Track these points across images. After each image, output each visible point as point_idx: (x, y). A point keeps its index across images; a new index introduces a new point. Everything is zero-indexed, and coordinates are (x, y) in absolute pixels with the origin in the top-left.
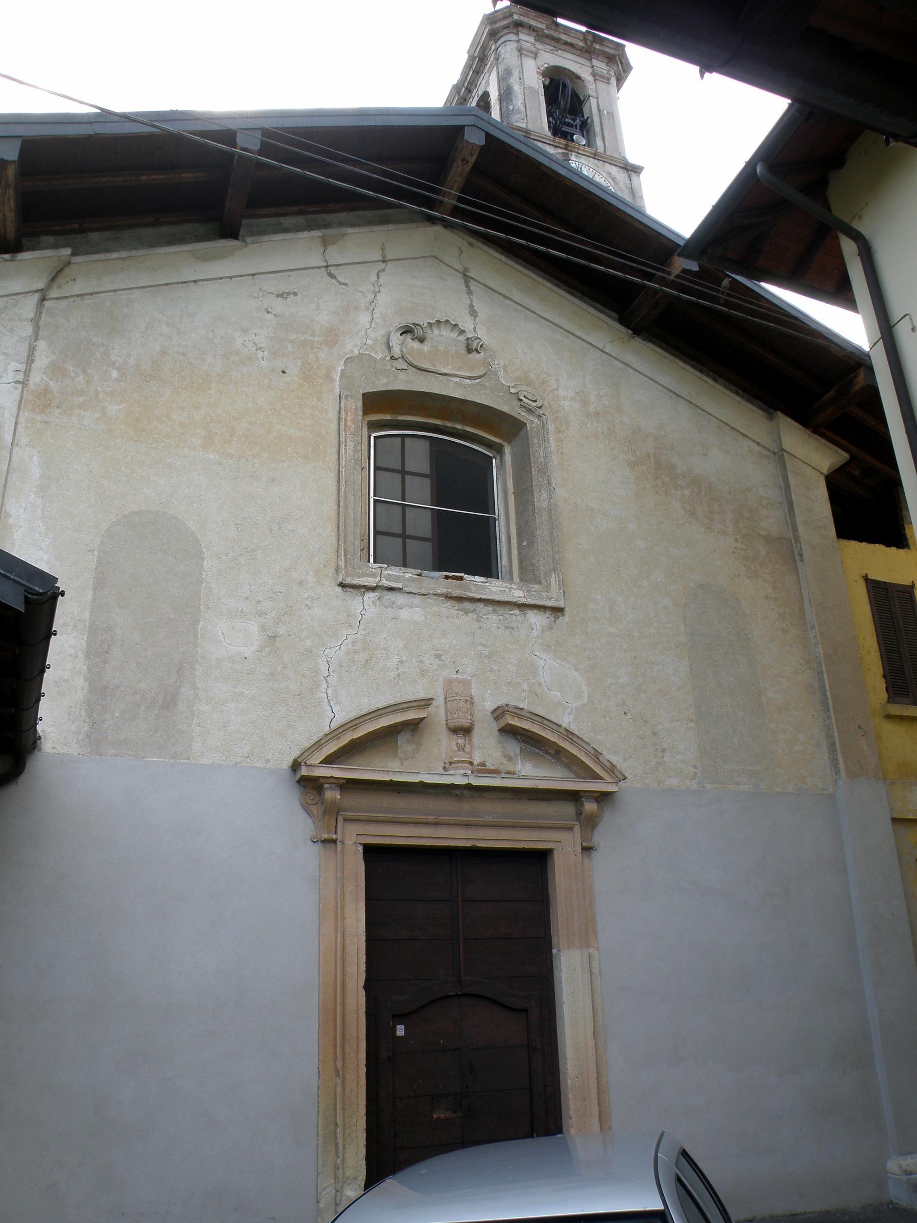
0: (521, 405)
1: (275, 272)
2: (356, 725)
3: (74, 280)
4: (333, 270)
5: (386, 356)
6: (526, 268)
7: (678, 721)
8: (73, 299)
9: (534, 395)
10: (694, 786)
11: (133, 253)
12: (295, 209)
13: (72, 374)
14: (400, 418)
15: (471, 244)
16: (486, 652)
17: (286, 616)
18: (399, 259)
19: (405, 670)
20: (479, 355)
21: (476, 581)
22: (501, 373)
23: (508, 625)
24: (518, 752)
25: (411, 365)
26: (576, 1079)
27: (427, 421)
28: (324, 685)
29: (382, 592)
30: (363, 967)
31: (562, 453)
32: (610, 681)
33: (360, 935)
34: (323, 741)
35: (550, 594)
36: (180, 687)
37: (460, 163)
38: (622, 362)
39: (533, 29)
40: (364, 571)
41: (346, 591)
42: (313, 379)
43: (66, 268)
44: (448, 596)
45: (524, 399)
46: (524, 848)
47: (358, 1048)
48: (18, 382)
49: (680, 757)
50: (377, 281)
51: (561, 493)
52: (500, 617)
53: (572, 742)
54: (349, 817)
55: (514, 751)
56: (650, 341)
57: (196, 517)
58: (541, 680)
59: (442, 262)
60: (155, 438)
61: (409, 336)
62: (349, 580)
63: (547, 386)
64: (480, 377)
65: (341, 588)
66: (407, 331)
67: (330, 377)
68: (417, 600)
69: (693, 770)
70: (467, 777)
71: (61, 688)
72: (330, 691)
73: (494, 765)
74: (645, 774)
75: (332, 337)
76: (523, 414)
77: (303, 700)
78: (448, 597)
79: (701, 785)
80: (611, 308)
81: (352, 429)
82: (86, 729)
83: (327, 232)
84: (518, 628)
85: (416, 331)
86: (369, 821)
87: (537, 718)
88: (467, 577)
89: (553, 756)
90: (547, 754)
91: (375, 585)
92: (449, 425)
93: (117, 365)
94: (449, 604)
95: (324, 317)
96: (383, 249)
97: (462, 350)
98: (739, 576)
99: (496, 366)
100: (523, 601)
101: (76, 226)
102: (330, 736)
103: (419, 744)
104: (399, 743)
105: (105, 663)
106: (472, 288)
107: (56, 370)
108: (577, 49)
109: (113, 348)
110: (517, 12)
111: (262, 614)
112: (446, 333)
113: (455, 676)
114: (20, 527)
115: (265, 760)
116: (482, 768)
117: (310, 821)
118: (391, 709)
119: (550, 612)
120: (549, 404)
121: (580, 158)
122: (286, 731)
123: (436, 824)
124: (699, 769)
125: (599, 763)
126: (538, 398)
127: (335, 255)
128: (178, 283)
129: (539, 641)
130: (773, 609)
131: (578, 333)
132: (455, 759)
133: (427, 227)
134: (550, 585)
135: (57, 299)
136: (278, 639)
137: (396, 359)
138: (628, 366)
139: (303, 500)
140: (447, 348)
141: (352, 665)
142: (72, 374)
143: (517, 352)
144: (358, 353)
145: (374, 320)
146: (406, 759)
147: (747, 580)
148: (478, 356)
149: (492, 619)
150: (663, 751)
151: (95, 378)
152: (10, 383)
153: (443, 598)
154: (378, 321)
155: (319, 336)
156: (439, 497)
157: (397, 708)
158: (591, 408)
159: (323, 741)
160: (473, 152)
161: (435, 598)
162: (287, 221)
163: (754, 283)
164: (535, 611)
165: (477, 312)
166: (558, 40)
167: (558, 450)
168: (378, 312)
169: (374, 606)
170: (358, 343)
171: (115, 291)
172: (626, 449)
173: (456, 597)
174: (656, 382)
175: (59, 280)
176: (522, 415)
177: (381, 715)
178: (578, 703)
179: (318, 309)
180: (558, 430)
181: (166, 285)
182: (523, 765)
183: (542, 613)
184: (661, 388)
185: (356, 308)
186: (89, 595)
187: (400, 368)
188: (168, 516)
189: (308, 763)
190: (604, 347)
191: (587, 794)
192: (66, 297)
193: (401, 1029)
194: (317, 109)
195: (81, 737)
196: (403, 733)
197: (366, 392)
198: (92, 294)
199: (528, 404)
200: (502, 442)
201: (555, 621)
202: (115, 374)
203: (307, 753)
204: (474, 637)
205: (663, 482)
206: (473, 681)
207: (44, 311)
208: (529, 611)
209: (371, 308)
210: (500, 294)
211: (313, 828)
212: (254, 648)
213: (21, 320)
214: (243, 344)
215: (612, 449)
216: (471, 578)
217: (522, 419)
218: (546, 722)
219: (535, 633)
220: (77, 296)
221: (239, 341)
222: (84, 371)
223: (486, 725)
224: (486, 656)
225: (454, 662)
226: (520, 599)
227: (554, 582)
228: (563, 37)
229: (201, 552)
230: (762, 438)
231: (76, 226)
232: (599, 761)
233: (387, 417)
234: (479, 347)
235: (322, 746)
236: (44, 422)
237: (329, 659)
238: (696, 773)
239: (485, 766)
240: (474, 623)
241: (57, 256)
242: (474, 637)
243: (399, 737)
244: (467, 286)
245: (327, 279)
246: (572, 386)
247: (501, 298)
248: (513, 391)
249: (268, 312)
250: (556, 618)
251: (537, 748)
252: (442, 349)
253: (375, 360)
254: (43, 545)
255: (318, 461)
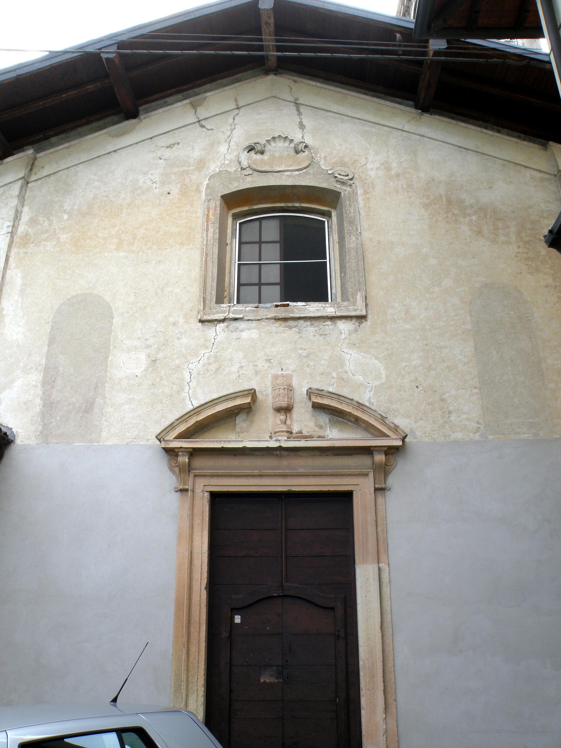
0: (336, 181)
1: (165, 133)
2: (199, 412)
3: (43, 167)
4: (203, 123)
5: (238, 169)
6: (341, 88)
7: (463, 389)
8: (44, 179)
9: (345, 172)
10: (477, 437)
11: (72, 143)
12: (173, 90)
13: (42, 222)
14: (255, 207)
15: (295, 81)
16: (305, 353)
17: (164, 346)
18: (248, 105)
19: (244, 372)
20: (305, 153)
21: (298, 306)
22: (322, 163)
23: (322, 333)
24: (327, 421)
25: (255, 171)
26: (367, 661)
27: (275, 206)
28: (187, 388)
29: (229, 323)
30: (205, 575)
31: (369, 208)
32: (404, 364)
33: (204, 553)
34: (175, 424)
35: (356, 307)
36: (95, 398)
37: (265, 27)
38: (418, 135)
40: (217, 310)
41: (205, 325)
42: (187, 194)
43: (35, 161)
44: (276, 318)
45: (338, 176)
46: (329, 490)
47: (199, 630)
48: (8, 233)
49: (464, 416)
50: (233, 122)
51: (366, 235)
52: (316, 328)
53: (364, 411)
54: (198, 474)
55: (325, 422)
56: (435, 113)
57: (110, 293)
58: (347, 369)
59: (279, 99)
60: (87, 250)
61: (252, 153)
62: (206, 318)
63: (358, 164)
64: (306, 168)
65: (201, 323)
66: (251, 149)
67: (199, 190)
68: (254, 324)
69: (476, 425)
70: (279, 442)
71: (27, 406)
72: (191, 392)
73: (308, 432)
74: (433, 431)
75: (201, 164)
76: (338, 186)
77: (172, 399)
78: (277, 319)
79: (483, 437)
80: (407, 99)
81: (213, 220)
82: (40, 429)
83: (192, 99)
84: (330, 334)
85: (256, 147)
86: (212, 476)
87: (335, 396)
88: (292, 304)
89: (354, 423)
90: (349, 422)
91: (223, 318)
92: (290, 205)
93: (68, 211)
94: (278, 324)
95: (197, 153)
96: (236, 100)
97: (292, 152)
98: (521, 273)
99: (318, 158)
100: (333, 314)
101: (42, 136)
102: (180, 420)
103: (252, 422)
104: (237, 422)
105: (52, 388)
106: (301, 110)
107: (33, 221)
109: (65, 202)
111: (149, 347)
112: (280, 144)
113: (281, 373)
114: (9, 315)
115: (146, 440)
116: (300, 435)
117: (174, 478)
118: (223, 399)
119: (356, 320)
120: (359, 176)
122: (161, 420)
123: (261, 476)
124: (482, 424)
125: (385, 425)
126: (350, 173)
127: (203, 112)
128: (104, 155)
129: (347, 341)
130: (553, 295)
131: (382, 122)
132: (277, 430)
133: (263, 78)
134: (356, 300)
135: (35, 181)
136: (158, 362)
137: (245, 169)
138: (424, 136)
139: (178, 271)
140: (281, 154)
141: (207, 372)
142: (42, 222)
143: (335, 146)
144: (218, 171)
145: (230, 148)
146: (242, 433)
147: (529, 276)
148: (304, 154)
149: (310, 330)
150: (450, 412)
151: (55, 221)
152: (4, 234)
153: (274, 321)
154: (233, 147)
155: (193, 166)
156: (285, 255)
157: (227, 397)
158: (393, 172)
159: (175, 424)
160: (269, 16)
161: (267, 321)
162: (168, 100)
163: (489, 41)
164: (343, 321)
165: (305, 126)
167: (366, 206)
168: (233, 141)
169: (224, 332)
170: (219, 164)
171: (68, 168)
172: (421, 195)
173: (282, 318)
174: (448, 143)
175: (34, 170)
176: (338, 187)
177: (217, 404)
178: (377, 383)
179: (193, 149)
180: (366, 193)
181: (98, 157)
182: (331, 431)
183: (349, 321)
184: (452, 147)
185: (219, 143)
186: (46, 349)
187: (247, 174)
188: (93, 295)
189: (166, 439)
190: (403, 127)
191: (376, 449)
192: (40, 179)
193: (238, 618)
195: (37, 434)
196: (240, 415)
197: (223, 194)
198: (54, 173)
199: (341, 179)
200: (330, 209)
201: (359, 326)
202: (66, 217)
203: (164, 433)
204: (296, 344)
205: (453, 214)
206: (294, 375)
207: (28, 189)
208: (339, 321)
209: (228, 140)
210: (322, 109)
211: (176, 482)
212: (142, 369)
213: (12, 197)
214: (144, 182)
215: (410, 197)
216: (295, 304)
217: (338, 190)
218: (341, 398)
219: (343, 336)
220: (46, 176)
221: (142, 181)
222: (48, 219)
223: (303, 405)
224: (304, 357)
225: (280, 363)
226: (331, 314)
227: (359, 298)
229: (112, 313)
230: (543, 165)
231: (42, 136)
232: (385, 423)
233: (246, 208)
234: (303, 148)
235: (175, 427)
236: (25, 253)
237: (191, 371)
238: (479, 428)
239: (302, 433)
240: (296, 335)
241: (26, 155)
242: (296, 344)
243: (237, 418)
244: (298, 110)
245: (199, 129)
246: (377, 160)
247: (323, 112)
248: (330, 172)
249: (161, 159)
250: (360, 323)
251: (341, 417)
252: (277, 155)
253: (230, 173)
254: (21, 324)
255: (190, 245)
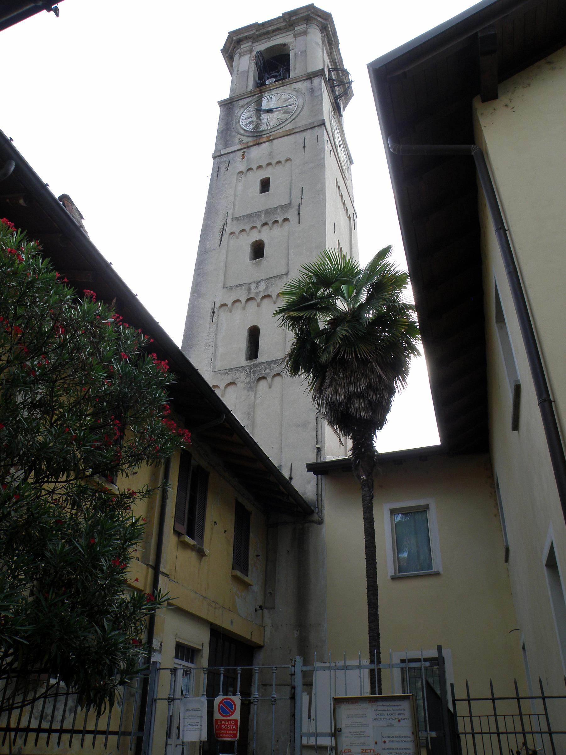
39: (249, 37)
108: (283, 29)
110: (234, 35)
121: (271, 92)
166: (268, 33)
194: (358, 249)
228: (270, 28)
